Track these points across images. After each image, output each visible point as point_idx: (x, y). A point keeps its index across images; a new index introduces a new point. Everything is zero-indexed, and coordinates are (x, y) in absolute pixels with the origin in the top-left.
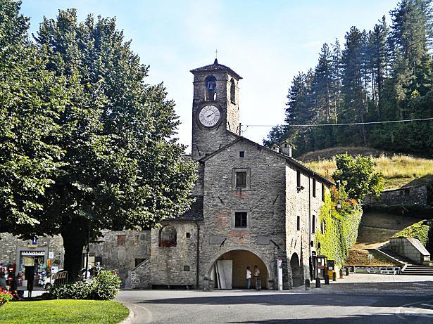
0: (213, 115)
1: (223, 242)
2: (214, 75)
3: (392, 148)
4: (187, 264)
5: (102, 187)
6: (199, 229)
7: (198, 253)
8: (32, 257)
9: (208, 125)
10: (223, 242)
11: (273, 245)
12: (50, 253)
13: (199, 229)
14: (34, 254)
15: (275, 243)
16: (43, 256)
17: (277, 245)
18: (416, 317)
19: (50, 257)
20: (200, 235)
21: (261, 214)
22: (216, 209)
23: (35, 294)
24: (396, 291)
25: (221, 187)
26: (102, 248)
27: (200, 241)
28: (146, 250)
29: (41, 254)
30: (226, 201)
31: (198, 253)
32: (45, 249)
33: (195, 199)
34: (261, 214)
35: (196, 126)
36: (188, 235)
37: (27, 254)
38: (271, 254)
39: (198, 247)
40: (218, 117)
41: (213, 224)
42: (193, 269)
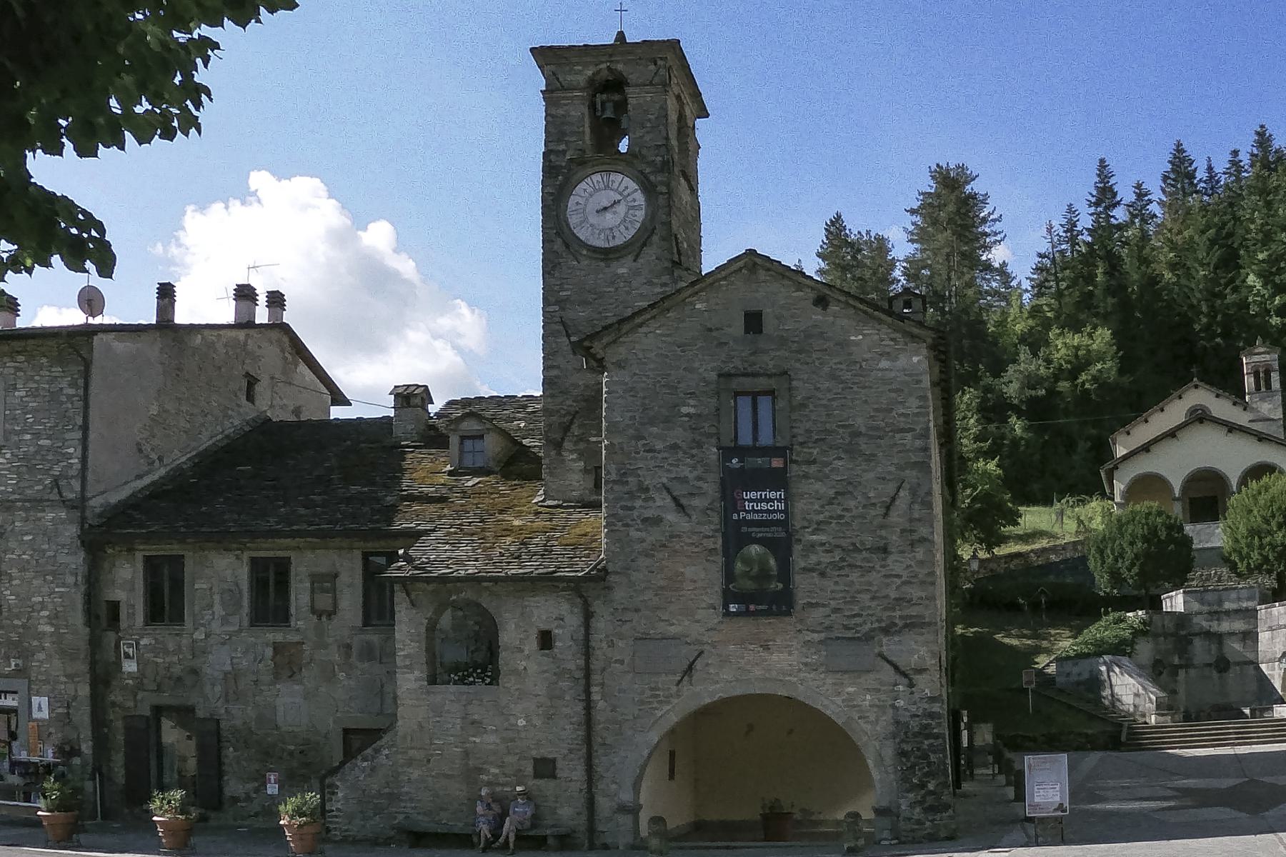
0: (621, 209)
1: (690, 667)
4: (547, 752)
5: (924, 743)
6: (588, 616)
9: (600, 243)
10: (690, 667)
11: (888, 674)
12: (35, 700)
13: (588, 616)
15: (896, 668)
16: (13, 711)
17: (905, 675)
18: (1129, 814)
19: (36, 715)
21: (837, 555)
22: (654, 535)
25: (674, 447)
26: (218, 688)
27: (596, 665)
28: (383, 693)
30: (696, 502)
31: (589, 706)
32: (20, 684)
33: (1120, 451)
34: (837, 555)
35: (558, 245)
36: (546, 640)
38: (882, 708)
40: (640, 215)
41: (648, 595)
42: (572, 771)
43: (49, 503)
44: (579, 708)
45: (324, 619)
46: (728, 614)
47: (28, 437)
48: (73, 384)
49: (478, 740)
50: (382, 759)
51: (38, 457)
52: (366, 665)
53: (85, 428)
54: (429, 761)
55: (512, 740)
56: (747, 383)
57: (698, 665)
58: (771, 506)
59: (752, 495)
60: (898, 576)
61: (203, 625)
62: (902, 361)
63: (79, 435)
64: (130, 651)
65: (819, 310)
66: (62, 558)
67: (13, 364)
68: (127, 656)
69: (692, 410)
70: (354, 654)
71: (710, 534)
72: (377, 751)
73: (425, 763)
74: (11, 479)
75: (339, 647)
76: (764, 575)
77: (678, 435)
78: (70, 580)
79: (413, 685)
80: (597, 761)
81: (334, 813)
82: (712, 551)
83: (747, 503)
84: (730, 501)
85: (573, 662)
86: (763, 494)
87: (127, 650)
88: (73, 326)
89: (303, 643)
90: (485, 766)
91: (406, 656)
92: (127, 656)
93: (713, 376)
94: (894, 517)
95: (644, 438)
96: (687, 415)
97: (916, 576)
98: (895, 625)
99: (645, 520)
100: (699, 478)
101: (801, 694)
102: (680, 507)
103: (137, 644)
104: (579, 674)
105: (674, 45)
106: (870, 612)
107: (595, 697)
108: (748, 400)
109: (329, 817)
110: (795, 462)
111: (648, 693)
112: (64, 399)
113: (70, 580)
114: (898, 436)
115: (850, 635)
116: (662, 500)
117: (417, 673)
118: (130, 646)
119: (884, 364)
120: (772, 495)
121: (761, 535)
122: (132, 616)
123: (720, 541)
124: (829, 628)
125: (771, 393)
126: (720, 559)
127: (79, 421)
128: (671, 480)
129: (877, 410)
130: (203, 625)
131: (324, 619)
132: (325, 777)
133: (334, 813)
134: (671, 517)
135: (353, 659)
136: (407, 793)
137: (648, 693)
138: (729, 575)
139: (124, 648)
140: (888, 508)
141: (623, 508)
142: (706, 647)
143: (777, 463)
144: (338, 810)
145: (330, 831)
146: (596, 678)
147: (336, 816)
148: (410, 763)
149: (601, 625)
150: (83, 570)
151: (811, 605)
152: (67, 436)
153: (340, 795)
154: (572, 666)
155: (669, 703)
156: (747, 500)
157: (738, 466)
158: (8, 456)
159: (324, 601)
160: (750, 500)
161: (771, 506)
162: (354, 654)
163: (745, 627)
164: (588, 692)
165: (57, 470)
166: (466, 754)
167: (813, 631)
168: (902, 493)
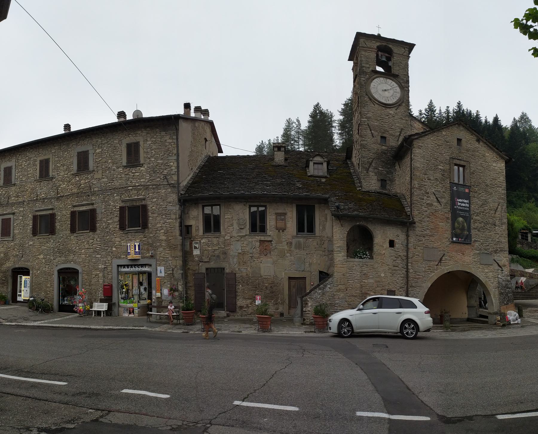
1: (441, 260)
2: (390, 46)
3: (174, 315)
6: (408, 236)
7: (407, 272)
8: (134, 273)
10: (441, 260)
12: (159, 268)
13: (408, 236)
14: (137, 269)
19: (159, 275)
20: (410, 245)
23: (173, 164)
24: (356, 334)
25: (436, 179)
26: (235, 260)
27: (410, 255)
29: (146, 269)
31: (407, 272)
34: (482, 225)
36: (392, 244)
37: (126, 269)
39: (407, 263)
41: (428, 232)
43: (163, 186)
44: (404, 271)
45: (281, 231)
46: (454, 242)
47: (153, 159)
48: (171, 138)
49: (366, 281)
50: (327, 289)
51: (158, 167)
52: (297, 251)
53: (178, 155)
54: (347, 290)
55: (379, 282)
56: (458, 162)
57: (443, 259)
58: (465, 205)
59: (460, 200)
60: (498, 234)
61: (229, 233)
62: (499, 165)
63: (175, 158)
64: (197, 246)
65: (477, 143)
66: (169, 208)
67: (146, 131)
68: (196, 248)
69: (442, 168)
70: (293, 246)
71: (447, 212)
72: (326, 286)
73: (345, 290)
74: (147, 176)
75: (287, 243)
76: (463, 229)
77: (438, 175)
78: (173, 217)
79: (341, 259)
80: (409, 292)
81: (307, 312)
82: (448, 218)
83: (458, 203)
84: (453, 203)
85: (403, 253)
86: (463, 200)
87: (195, 245)
88: (169, 115)
89: (272, 241)
90: (368, 292)
91: (338, 247)
92: (196, 248)
93: (448, 158)
94: (497, 215)
95: (427, 175)
96: (440, 169)
97: (503, 235)
98: (498, 250)
99: (428, 204)
100: (444, 192)
101: (473, 271)
102: (438, 201)
103: (200, 242)
104: (404, 258)
105: (359, 36)
106: (492, 245)
107: (409, 267)
108: (137, 276)
109: (305, 314)
110: (472, 191)
111: (427, 268)
112: (167, 144)
113: (173, 217)
114: (498, 189)
115: (486, 252)
116: (433, 198)
117: (343, 254)
118: (196, 243)
119: (494, 165)
120: (466, 201)
121: (462, 214)
122: (197, 230)
123: (450, 215)
124: (480, 250)
125: (463, 166)
126: (450, 221)
127: (175, 152)
128: (435, 191)
129: (493, 179)
130: (229, 233)
131: (281, 231)
132: (303, 297)
133: (307, 312)
134: (436, 204)
135: (293, 249)
136: (337, 303)
137: (427, 268)
138: (453, 228)
139: (194, 245)
140: (496, 211)
141: (420, 198)
142: (446, 253)
143: (467, 191)
144: (309, 311)
145: (305, 320)
146: (410, 261)
147: (308, 314)
148: (339, 290)
149: (412, 240)
150: (179, 212)
151: (475, 241)
152: (170, 158)
153: (310, 304)
154: (401, 254)
155: (434, 272)
156: (458, 202)
157: (456, 190)
158: (146, 167)
159: (281, 224)
160: (459, 202)
161: (465, 205)
162: (293, 246)
163: (458, 247)
164: (407, 266)
165: (165, 172)
166: (362, 286)
167: (476, 250)
168: (499, 207)
